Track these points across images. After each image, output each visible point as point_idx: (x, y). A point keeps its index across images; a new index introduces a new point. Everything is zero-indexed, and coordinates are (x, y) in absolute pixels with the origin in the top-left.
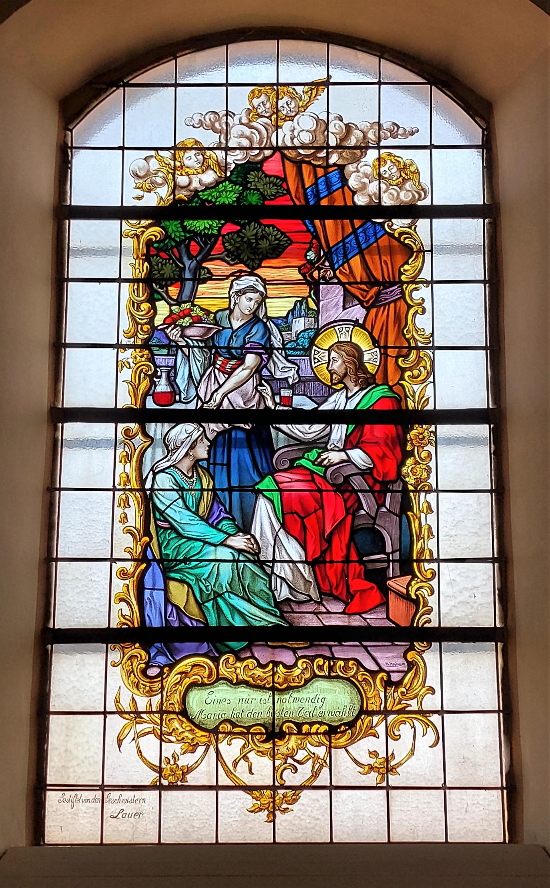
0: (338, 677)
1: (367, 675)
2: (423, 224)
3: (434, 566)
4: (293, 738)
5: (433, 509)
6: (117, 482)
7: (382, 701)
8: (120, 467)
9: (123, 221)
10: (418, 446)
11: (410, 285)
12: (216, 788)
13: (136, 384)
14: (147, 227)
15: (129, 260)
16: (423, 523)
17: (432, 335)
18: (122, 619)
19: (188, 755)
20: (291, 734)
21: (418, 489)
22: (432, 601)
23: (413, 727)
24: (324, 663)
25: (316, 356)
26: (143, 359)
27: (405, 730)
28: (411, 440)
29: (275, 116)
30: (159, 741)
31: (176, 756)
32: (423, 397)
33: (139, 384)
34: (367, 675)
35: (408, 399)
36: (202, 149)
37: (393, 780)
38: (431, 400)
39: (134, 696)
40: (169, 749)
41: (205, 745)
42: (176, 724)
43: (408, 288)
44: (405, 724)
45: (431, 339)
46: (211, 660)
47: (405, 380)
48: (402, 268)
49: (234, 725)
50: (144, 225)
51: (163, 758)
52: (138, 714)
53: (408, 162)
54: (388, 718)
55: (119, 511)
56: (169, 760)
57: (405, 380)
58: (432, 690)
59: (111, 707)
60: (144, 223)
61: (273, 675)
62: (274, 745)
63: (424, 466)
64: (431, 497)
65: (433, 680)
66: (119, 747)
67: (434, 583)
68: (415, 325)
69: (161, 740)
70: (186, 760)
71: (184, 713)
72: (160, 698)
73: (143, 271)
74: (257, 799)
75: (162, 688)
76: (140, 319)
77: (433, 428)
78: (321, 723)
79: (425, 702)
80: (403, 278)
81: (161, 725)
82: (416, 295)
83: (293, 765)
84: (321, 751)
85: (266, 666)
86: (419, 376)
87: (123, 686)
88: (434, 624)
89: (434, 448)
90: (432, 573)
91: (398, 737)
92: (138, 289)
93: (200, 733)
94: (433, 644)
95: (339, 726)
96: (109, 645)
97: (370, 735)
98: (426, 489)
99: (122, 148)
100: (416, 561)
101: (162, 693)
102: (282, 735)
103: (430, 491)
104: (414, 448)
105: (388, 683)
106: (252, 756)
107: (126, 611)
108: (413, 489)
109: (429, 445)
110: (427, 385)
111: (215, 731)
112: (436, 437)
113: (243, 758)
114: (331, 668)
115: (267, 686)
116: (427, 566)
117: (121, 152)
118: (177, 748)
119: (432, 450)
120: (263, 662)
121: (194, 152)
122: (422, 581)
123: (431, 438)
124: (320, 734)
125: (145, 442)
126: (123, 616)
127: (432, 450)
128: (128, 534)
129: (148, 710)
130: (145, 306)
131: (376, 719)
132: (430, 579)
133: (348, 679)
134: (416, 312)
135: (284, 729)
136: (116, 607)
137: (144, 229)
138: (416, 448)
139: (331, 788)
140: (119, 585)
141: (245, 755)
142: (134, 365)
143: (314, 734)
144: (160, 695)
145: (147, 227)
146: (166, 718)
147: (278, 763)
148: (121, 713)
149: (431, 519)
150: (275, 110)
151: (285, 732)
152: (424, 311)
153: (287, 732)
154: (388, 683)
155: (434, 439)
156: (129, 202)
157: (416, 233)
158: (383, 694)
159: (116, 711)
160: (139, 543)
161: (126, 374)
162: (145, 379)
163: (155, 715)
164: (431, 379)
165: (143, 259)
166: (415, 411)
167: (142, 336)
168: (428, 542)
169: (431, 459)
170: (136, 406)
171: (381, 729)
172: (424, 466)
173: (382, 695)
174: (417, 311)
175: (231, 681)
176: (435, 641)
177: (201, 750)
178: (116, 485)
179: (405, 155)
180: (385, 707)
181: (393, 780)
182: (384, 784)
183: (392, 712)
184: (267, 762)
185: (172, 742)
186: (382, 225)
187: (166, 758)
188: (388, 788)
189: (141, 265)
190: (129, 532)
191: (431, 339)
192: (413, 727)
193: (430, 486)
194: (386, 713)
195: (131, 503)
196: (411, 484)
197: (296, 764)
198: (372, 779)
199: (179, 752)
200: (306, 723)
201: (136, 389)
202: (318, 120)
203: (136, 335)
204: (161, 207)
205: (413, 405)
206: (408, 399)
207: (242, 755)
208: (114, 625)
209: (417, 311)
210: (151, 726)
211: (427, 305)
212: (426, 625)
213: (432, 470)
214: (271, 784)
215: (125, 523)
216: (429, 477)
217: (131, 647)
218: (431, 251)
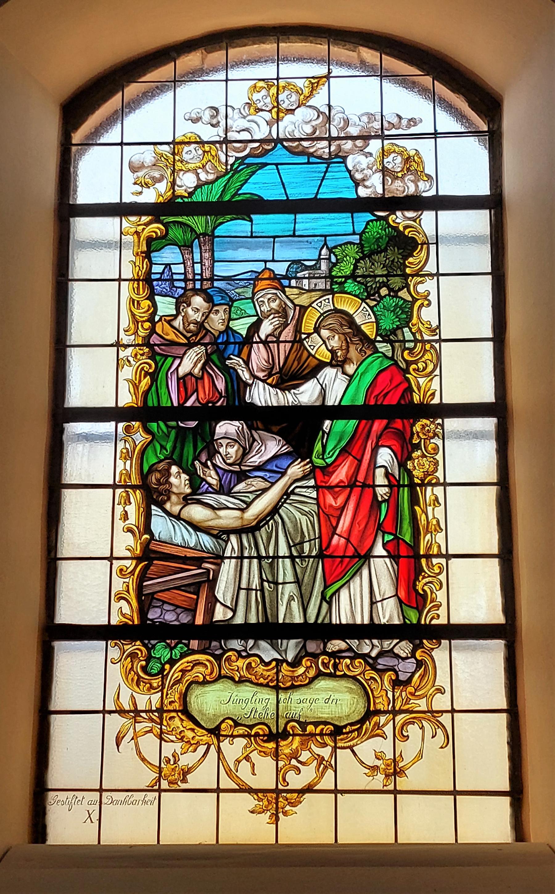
0: (345, 676)
1: (372, 673)
2: (428, 217)
3: (443, 561)
4: (297, 738)
5: (440, 501)
6: (117, 479)
7: (390, 701)
8: (120, 464)
9: (123, 218)
10: (424, 439)
11: (415, 278)
12: (218, 791)
13: (137, 382)
14: (147, 224)
15: (128, 255)
16: (430, 517)
17: (439, 327)
18: (121, 617)
19: (189, 754)
20: (294, 735)
21: (426, 482)
22: (441, 596)
23: (422, 728)
24: (330, 661)
25: (323, 302)
26: (144, 357)
27: (413, 730)
28: (418, 433)
29: (276, 109)
30: (159, 741)
31: (177, 755)
32: (429, 390)
33: (140, 381)
34: (372, 673)
35: (414, 393)
36: (202, 143)
37: (402, 783)
38: (438, 394)
39: (134, 693)
40: (168, 749)
41: (205, 744)
42: (177, 722)
43: (413, 281)
44: (414, 724)
45: (438, 331)
46: (212, 657)
47: (410, 374)
48: (406, 262)
49: (237, 724)
50: (146, 221)
51: (163, 757)
52: (137, 712)
53: (412, 153)
54: (396, 718)
55: (119, 509)
56: (170, 760)
57: (410, 374)
58: (441, 691)
59: (110, 706)
60: (145, 219)
61: (277, 673)
62: (278, 746)
63: (432, 459)
64: (439, 491)
65: (442, 680)
66: (118, 745)
67: (443, 577)
68: (419, 318)
69: (161, 739)
70: (186, 760)
71: (186, 712)
72: (160, 696)
73: (143, 268)
74: (260, 800)
75: (163, 685)
76: (140, 317)
77: (439, 421)
78: (326, 723)
79: (436, 698)
80: (408, 271)
81: (161, 724)
82: (421, 288)
83: (297, 767)
84: (326, 752)
85: (269, 663)
86: (424, 369)
87: (123, 686)
88: (442, 621)
89: (442, 441)
90: (439, 567)
91: (405, 739)
92: (138, 288)
93: (200, 731)
94: (442, 641)
95: (345, 726)
96: (109, 642)
97: (378, 735)
98: (433, 482)
99: (121, 144)
100: (425, 556)
101: (162, 691)
102: (285, 735)
103: (438, 484)
104: (420, 441)
105: (396, 683)
106: (254, 756)
107: (126, 610)
108: (420, 482)
109: (436, 437)
110: (433, 377)
111: (215, 732)
112: (443, 429)
113: (245, 758)
114: (335, 666)
115: (271, 684)
116: (435, 561)
117: (120, 147)
118: (178, 747)
119: (440, 443)
120: (267, 660)
121: (193, 146)
122: (429, 576)
123: (437, 430)
124: (326, 734)
125: (146, 439)
126: (124, 615)
127: (440, 443)
128: (129, 533)
129: (147, 709)
130: (146, 303)
131: (383, 719)
132: (439, 574)
133: (354, 678)
134: (422, 305)
135: (288, 729)
136: (115, 606)
137: (145, 227)
138: (423, 440)
139: (336, 791)
140: (119, 584)
141: (247, 755)
142: (134, 363)
143: (318, 735)
144: (160, 693)
145: (147, 224)
146: (166, 717)
147: (281, 764)
148: (121, 712)
149: (439, 512)
150: (276, 104)
151: (289, 732)
152: (429, 305)
153: (291, 732)
154: (396, 683)
155: (441, 431)
156: (128, 198)
157: (420, 226)
158: (392, 693)
159: (115, 709)
160: (139, 541)
161: (127, 372)
162: (145, 377)
163: (155, 714)
164: (437, 372)
165: (142, 256)
166: (421, 405)
167: (142, 333)
168: (435, 535)
169: (439, 451)
170: (136, 404)
171: (388, 730)
172: (432, 459)
173: (390, 695)
174: (422, 304)
175: (232, 679)
176: (445, 639)
177: (202, 749)
178: (116, 482)
179: (410, 145)
180: (394, 706)
181: (402, 783)
182: (391, 787)
183: (401, 712)
184: (270, 762)
185: (172, 741)
186: (385, 219)
187: (165, 757)
188: (395, 792)
189: (141, 263)
190: (130, 530)
191: (438, 331)
192: (422, 728)
193: (438, 478)
194: (395, 713)
195: (132, 500)
196: (418, 478)
197: (299, 765)
198: (378, 782)
199: (179, 751)
200: (311, 723)
201: (136, 387)
202: (319, 113)
203: (137, 332)
204: (160, 203)
205: (418, 400)
206: (414, 393)
207: (244, 755)
208: (114, 622)
209: (422, 304)
210: (150, 725)
211: (433, 298)
212: (434, 622)
213: (440, 463)
214: (274, 787)
215: (125, 520)
216: (436, 470)
217: (131, 643)
218: (437, 243)
